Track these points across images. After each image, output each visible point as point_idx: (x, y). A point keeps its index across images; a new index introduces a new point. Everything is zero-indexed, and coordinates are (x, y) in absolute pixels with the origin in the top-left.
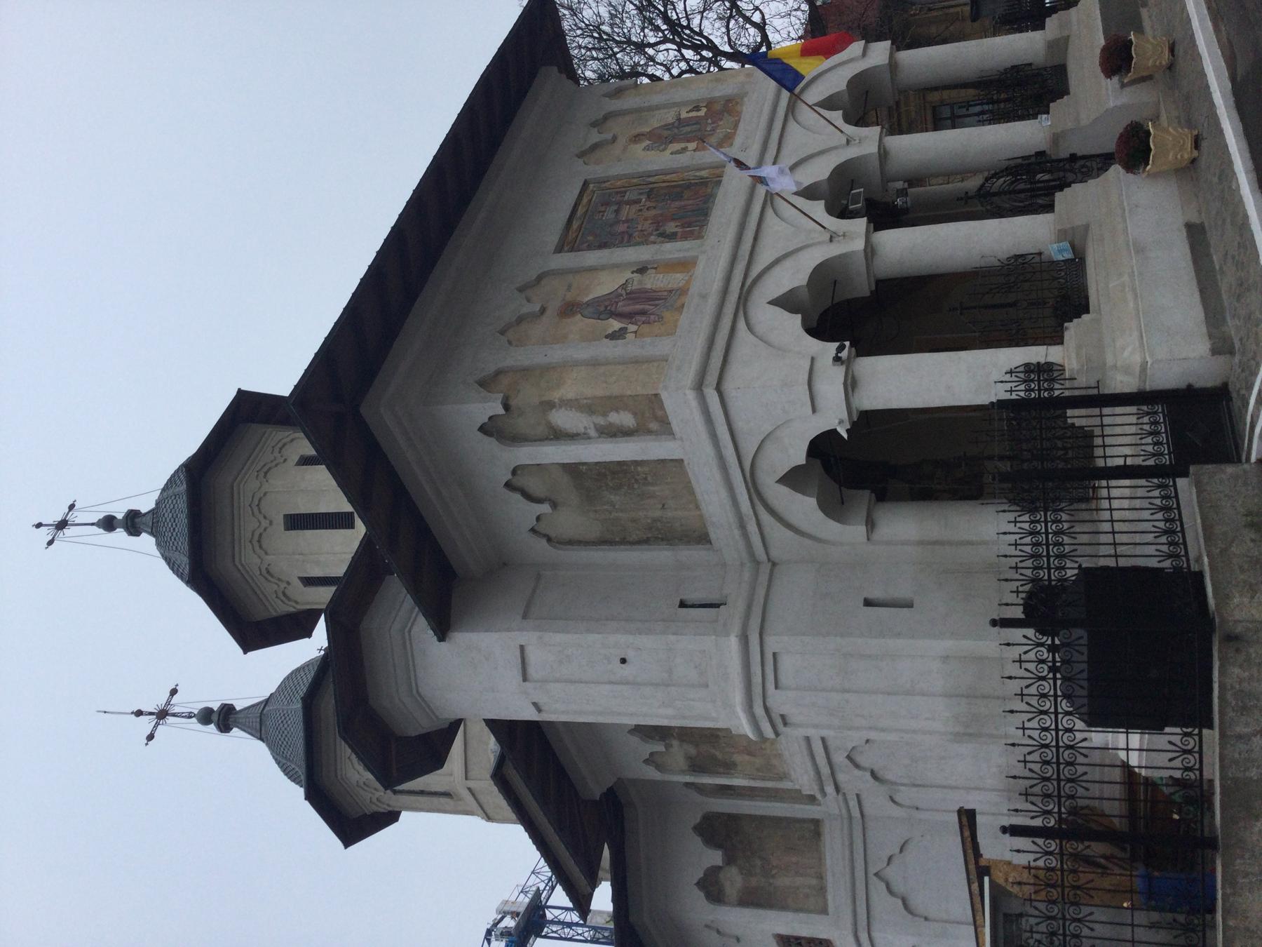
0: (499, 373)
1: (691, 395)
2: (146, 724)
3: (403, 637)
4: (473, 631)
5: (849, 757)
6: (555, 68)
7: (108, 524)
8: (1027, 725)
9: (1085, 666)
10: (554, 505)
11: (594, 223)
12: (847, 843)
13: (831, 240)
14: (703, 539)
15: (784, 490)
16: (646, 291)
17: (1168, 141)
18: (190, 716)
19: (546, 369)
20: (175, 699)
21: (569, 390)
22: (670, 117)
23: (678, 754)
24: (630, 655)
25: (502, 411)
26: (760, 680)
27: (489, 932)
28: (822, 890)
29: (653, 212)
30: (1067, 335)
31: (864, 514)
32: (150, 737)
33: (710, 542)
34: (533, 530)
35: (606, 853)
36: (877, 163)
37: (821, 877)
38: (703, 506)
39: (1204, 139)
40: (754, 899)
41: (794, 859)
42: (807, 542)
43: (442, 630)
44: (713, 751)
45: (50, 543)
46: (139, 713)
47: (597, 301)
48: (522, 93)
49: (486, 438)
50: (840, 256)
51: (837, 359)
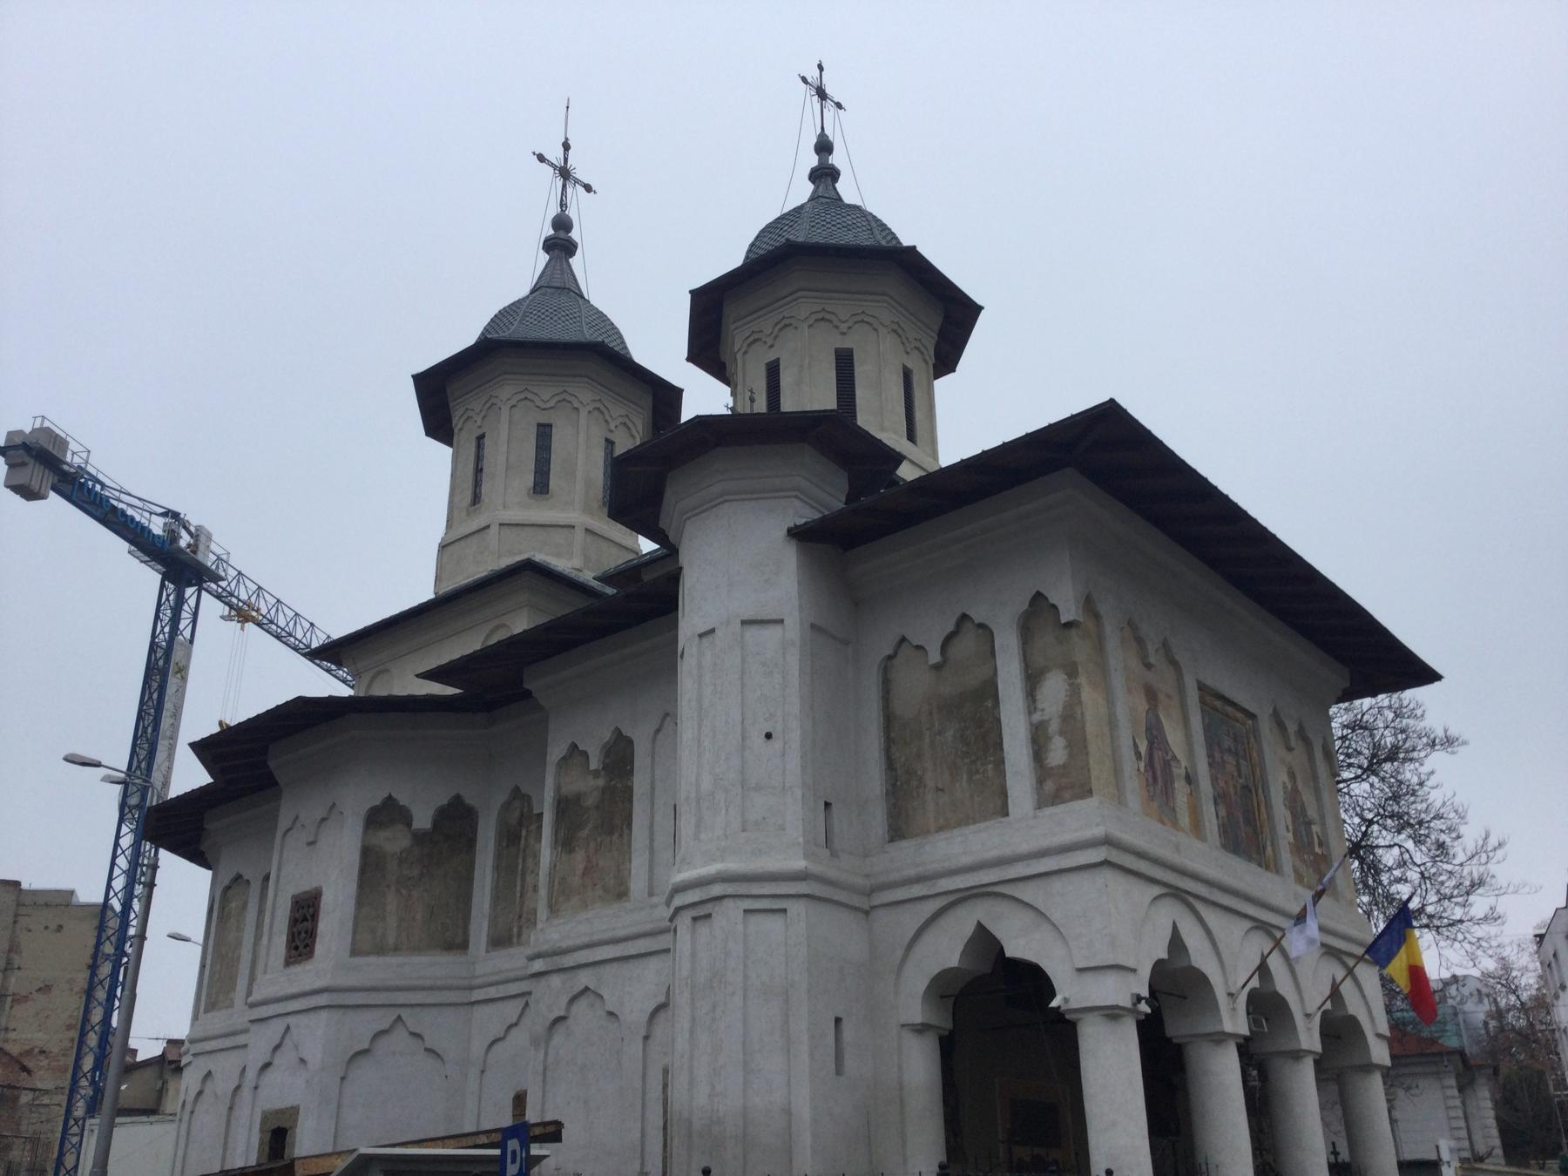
0: (1097, 617)
1: (1098, 831)
2: (555, 155)
5: (587, 989)
7: (824, 147)
10: (937, 667)
11: (1226, 722)
12: (439, 983)
14: (897, 832)
15: (969, 930)
16: (1172, 783)
18: (563, 205)
21: (1088, 695)
22: (1312, 813)
24: (776, 744)
25: (1063, 620)
27: (176, 516)
28: (380, 950)
29: (1232, 791)
31: (932, 1022)
32: (541, 158)
33: (892, 840)
34: (903, 639)
35: (450, 691)
37: (396, 949)
38: (942, 835)
40: (371, 864)
41: (419, 917)
42: (900, 953)
43: (798, 534)
44: (590, 825)
45: (804, 80)
46: (566, 146)
49: (1029, 597)
51: (1139, 999)
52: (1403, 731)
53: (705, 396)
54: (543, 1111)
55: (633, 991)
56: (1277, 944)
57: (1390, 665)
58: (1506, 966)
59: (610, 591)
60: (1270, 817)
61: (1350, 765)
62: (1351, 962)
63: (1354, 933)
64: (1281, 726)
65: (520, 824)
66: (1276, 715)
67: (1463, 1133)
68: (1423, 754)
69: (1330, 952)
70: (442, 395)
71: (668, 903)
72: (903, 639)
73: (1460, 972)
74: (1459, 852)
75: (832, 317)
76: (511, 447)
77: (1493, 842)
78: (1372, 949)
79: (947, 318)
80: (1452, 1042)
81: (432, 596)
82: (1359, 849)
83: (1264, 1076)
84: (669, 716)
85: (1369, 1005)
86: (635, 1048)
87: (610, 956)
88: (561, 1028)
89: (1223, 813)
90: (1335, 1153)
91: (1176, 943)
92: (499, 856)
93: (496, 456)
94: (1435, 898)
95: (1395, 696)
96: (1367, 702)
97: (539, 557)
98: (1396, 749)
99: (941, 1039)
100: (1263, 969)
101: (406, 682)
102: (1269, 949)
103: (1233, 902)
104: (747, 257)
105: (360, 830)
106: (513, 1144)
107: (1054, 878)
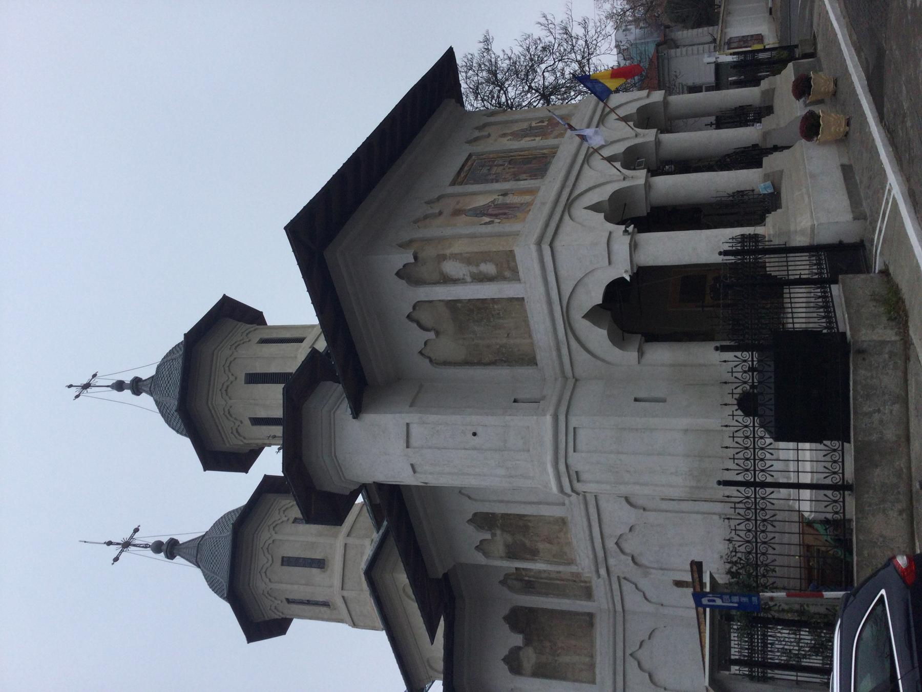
0: (411, 241)
1: (533, 248)
2: (114, 551)
3: (330, 416)
4: (376, 413)
5: (617, 543)
6: (454, 100)
7: (119, 386)
9: (772, 375)
10: (437, 333)
13: (624, 179)
14: (530, 360)
15: (587, 323)
17: (831, 121)
19: (441, 240)
22: (525, 125)
23: (500, 540)
24: (480, 430)
25: (413, 261)
26: (564, 446)
28: (592, 666)
29: (512, 170)
30: (767, 220)
32: (116, 559)
34: (420, 353)
35: (442, 623)
36: (654, 148)
37: (592, 656)
38: (534, 336)
39: (853, 120)
42: (599, 363)
43: (357, 412)
45: (77, 397)
46: (109, 543)
47: (475, 209)
48: (431, 111)
50: (628, 187)
51: (626, 231)
52: (480, 66)
53: (270, 462)
54: (685, 571)
55: (618, 517)
56: (596, 151)
57: (443, 77)
58: (610, 16)
59: (385, 523)
60: (528, 149)
61: (498, 97)
62: (607, 110)
63: (591, 107)
64: (476, 139)
65: (521, 580)
66: (469, 142)
67: (701, 47)
68: (493, 56)
69: (602, 120)
70: (261, 624)
71: (569, 496)
72: (420, 353)
73: (613, 44)
74: (548, 39)
75: (226, 410)
76: (295, 583)
77: (543, 20)
78: (601, 99)
79: (230, 316)
80: (651, 49)
81: (384, 633)
82: (545, 95)
83: (669, 162)
84: (461, 491)
85: (632, 100)
86: (651, 517)
87: (598, 529)
88: (638, 559)
89: (524, 176)
90: (711, 124)
91: (595, 208)
92: (539, 594)
93: (299, 591)
94: (573, 55)
95: (460, 69)
96: (464, 86)
97: (363, 566)
98: (489, 71)
99: (647, 341)
100: (610, 159)
101: (436, 649)
102: (598, 156)
103: (573, 175)
104: (185, 435)
105: (523, 679)
106: (705, 601)
107: (559, 274)
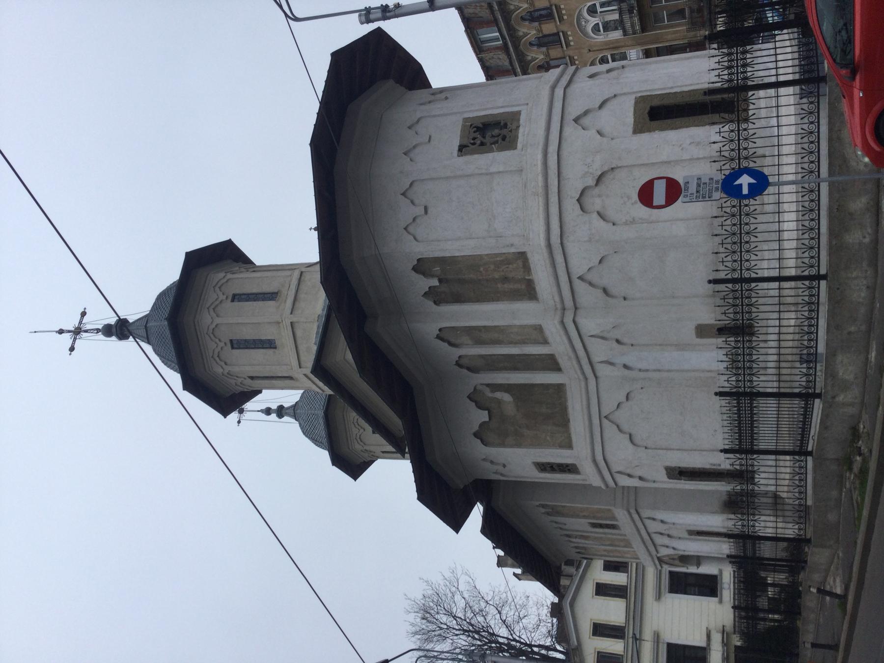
2: (67, 338)
8: (725, 259)
18: (98, 331)
20: (85, 320)
32: (72, 349)
46: (61, 332)
